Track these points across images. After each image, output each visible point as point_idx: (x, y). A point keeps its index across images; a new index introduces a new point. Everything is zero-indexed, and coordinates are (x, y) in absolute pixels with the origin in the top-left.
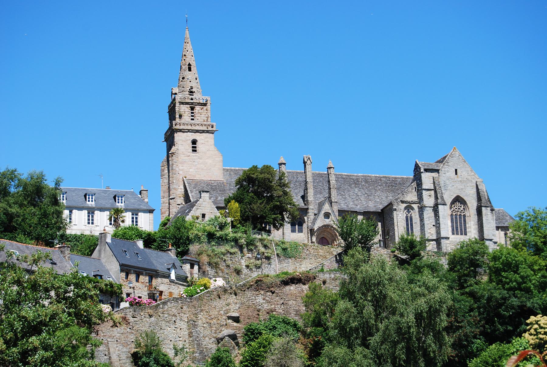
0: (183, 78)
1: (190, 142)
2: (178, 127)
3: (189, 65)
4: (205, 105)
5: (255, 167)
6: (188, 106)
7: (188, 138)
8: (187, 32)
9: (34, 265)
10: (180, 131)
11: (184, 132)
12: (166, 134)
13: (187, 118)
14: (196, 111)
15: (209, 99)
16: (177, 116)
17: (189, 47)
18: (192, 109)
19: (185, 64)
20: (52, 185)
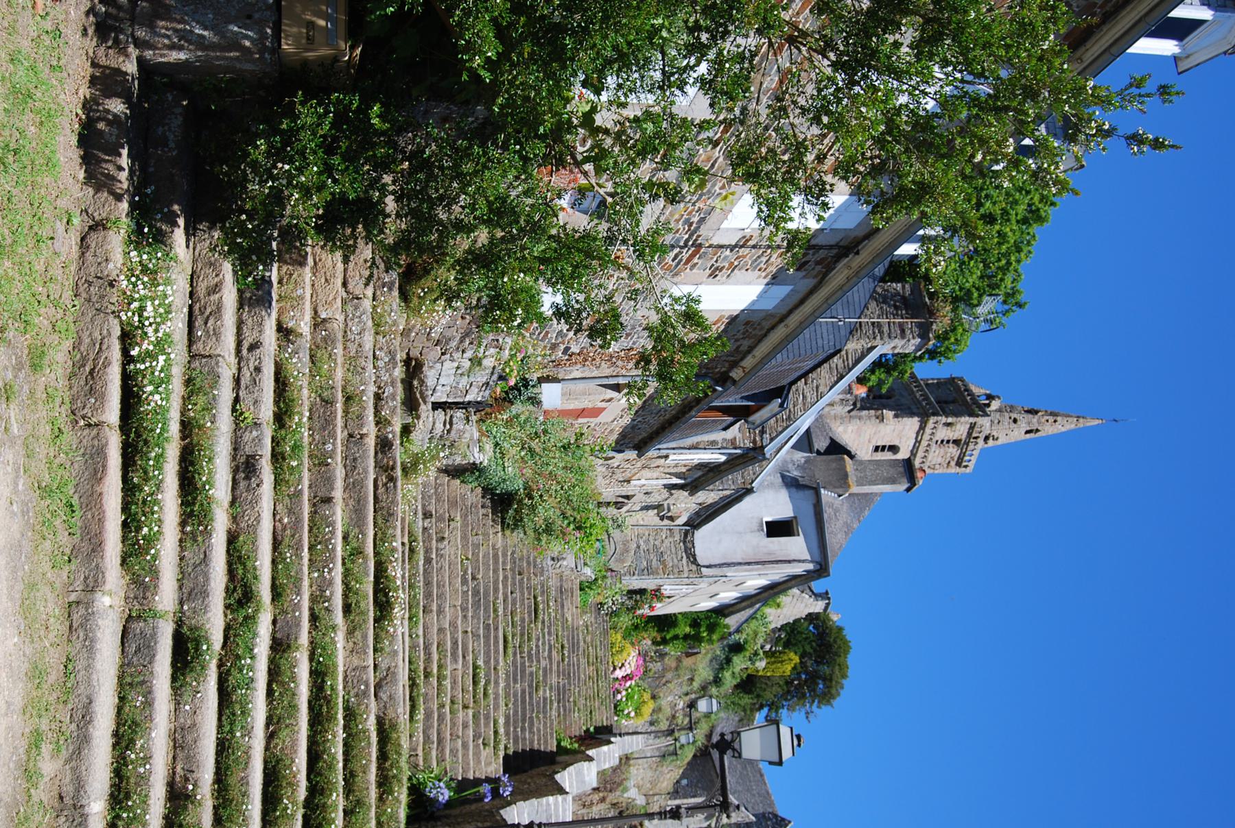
0: (1015, 421)
1: (896, 443)
2: (930, 424)
3: (1037, 430)
4: (959, 464)
5: (844, 676)
6: (964, 437)
7: (904, 440)
8: (1096, 422)
9: (654, 319)
10: (922, 428)
11: (918, 433)
12: (962, 380)
13: (943, 433)
14: (951, 450)
15: (968, 470)
16: (950, 420)
17: (1064, 426)
18: (956, 442)
19: (1039, 423)
20: (590, 753)
